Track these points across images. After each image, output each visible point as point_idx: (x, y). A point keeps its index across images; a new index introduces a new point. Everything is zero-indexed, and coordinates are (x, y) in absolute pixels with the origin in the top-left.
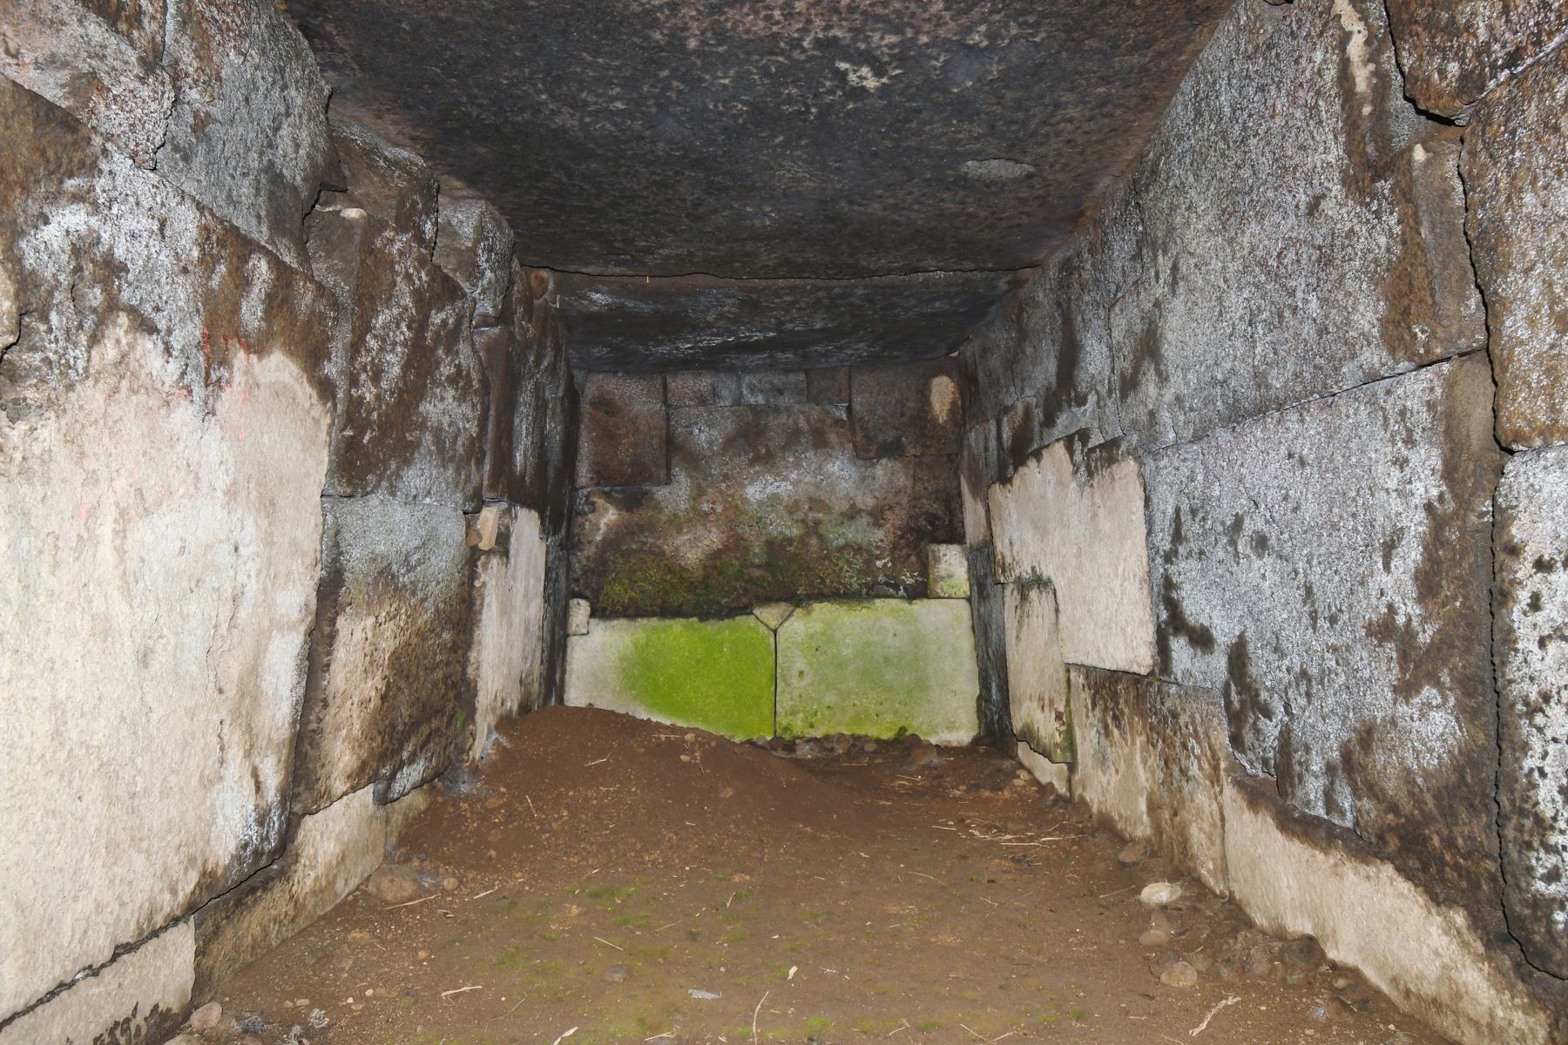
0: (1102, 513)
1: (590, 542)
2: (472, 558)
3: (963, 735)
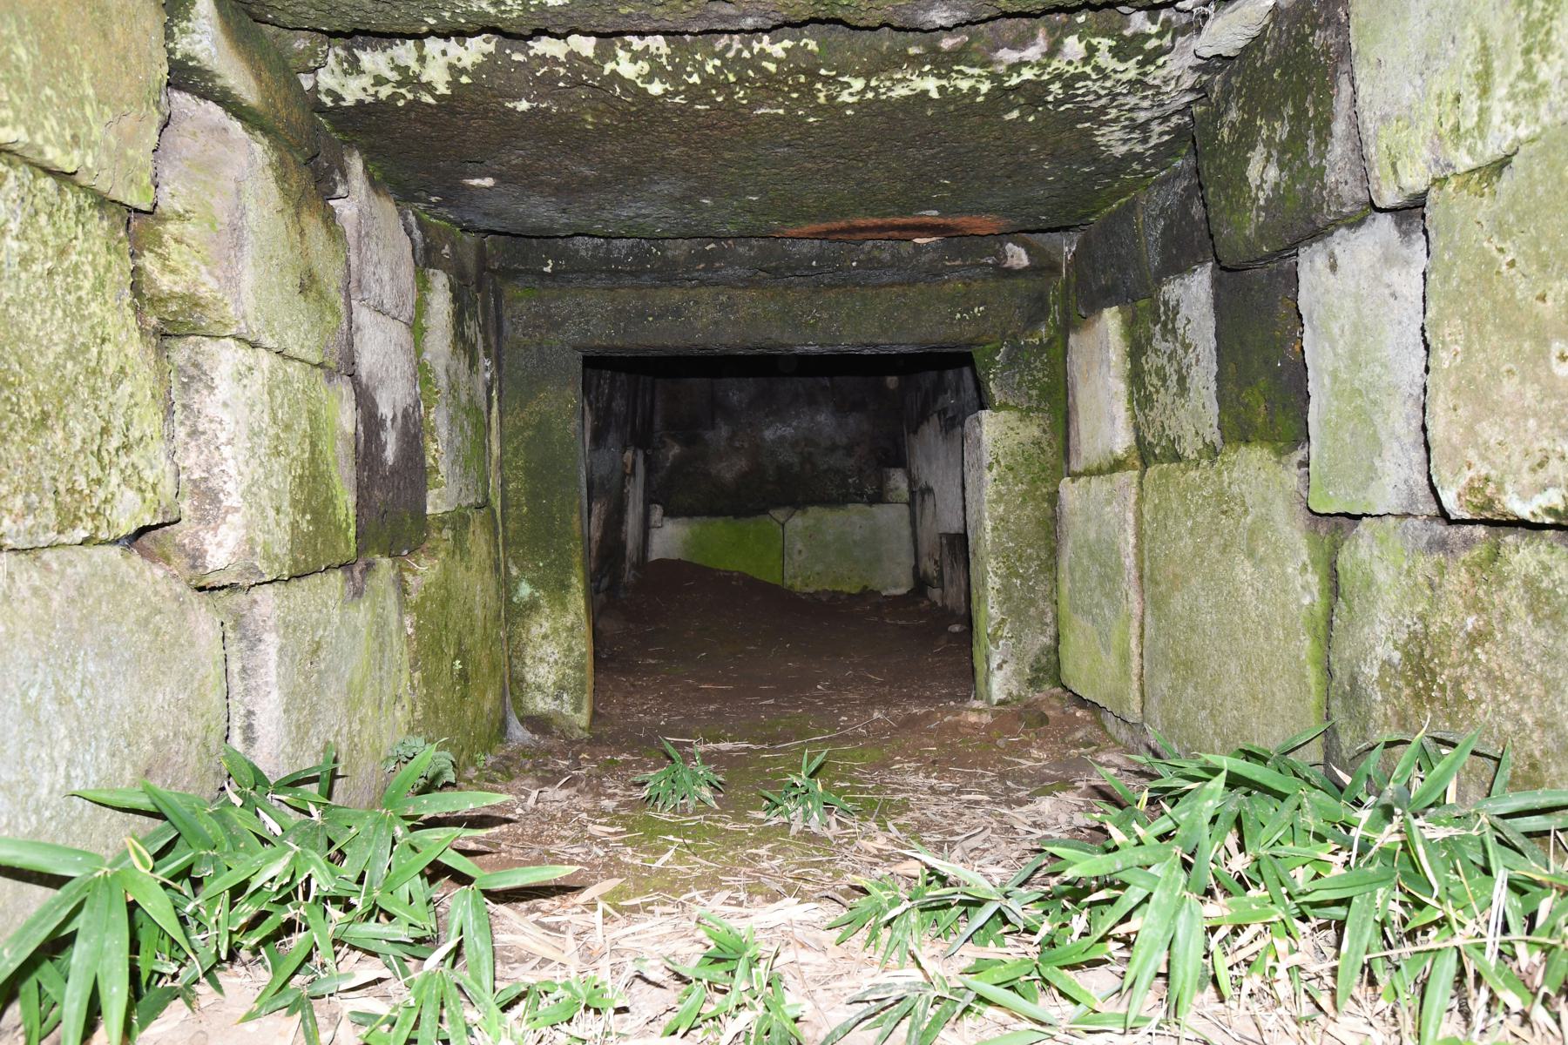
3: (902, 591)
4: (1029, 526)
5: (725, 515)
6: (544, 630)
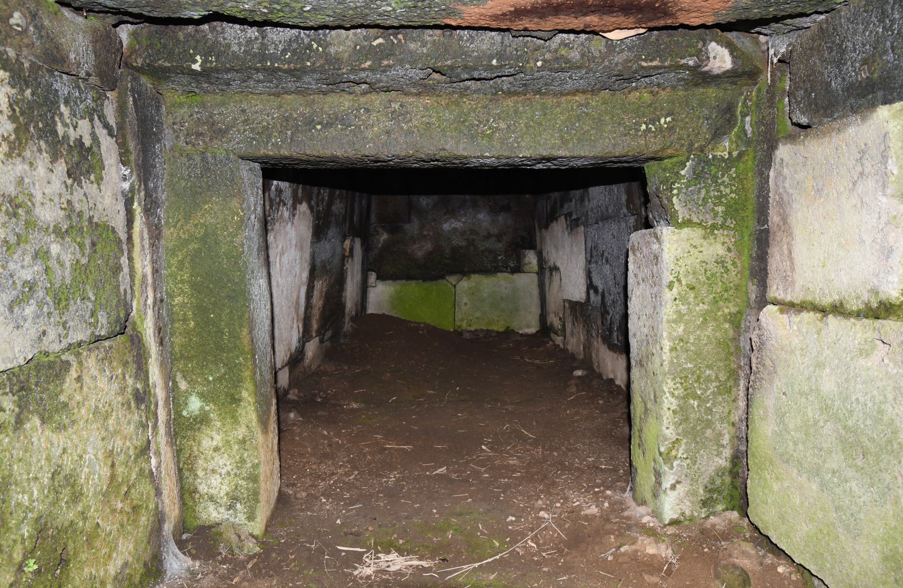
0: (574, 244)
1: (376, 248)
2: (343, 258)
3: (532, 330)
4: (709, 347)
5: (417, 279)
6: (215, 443)
